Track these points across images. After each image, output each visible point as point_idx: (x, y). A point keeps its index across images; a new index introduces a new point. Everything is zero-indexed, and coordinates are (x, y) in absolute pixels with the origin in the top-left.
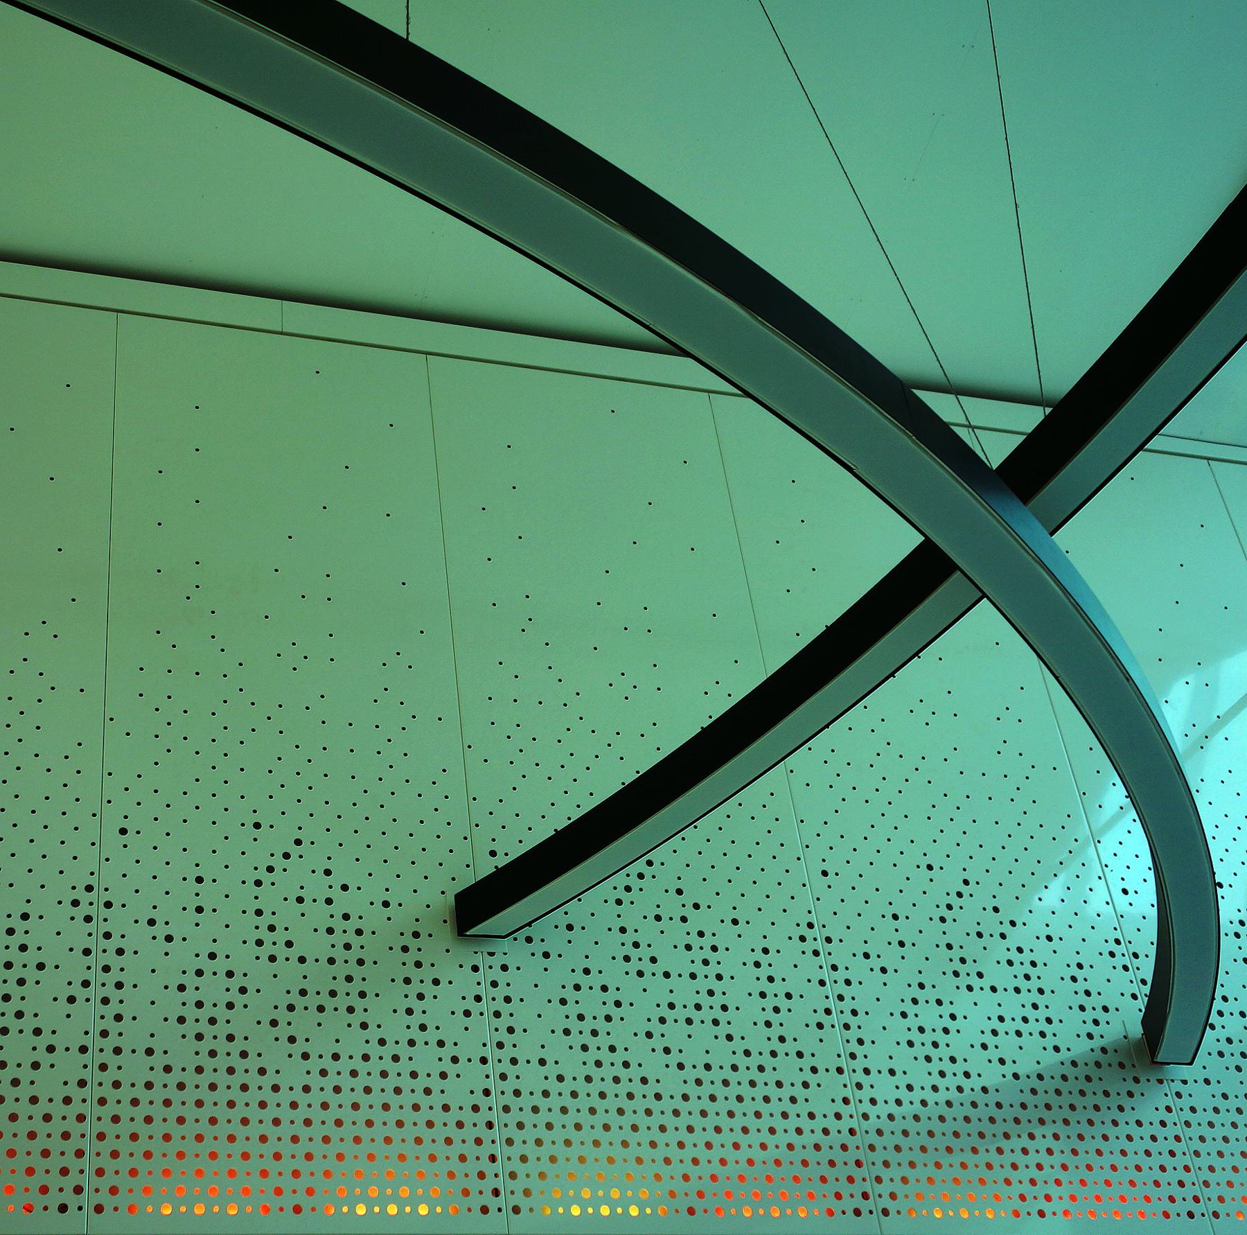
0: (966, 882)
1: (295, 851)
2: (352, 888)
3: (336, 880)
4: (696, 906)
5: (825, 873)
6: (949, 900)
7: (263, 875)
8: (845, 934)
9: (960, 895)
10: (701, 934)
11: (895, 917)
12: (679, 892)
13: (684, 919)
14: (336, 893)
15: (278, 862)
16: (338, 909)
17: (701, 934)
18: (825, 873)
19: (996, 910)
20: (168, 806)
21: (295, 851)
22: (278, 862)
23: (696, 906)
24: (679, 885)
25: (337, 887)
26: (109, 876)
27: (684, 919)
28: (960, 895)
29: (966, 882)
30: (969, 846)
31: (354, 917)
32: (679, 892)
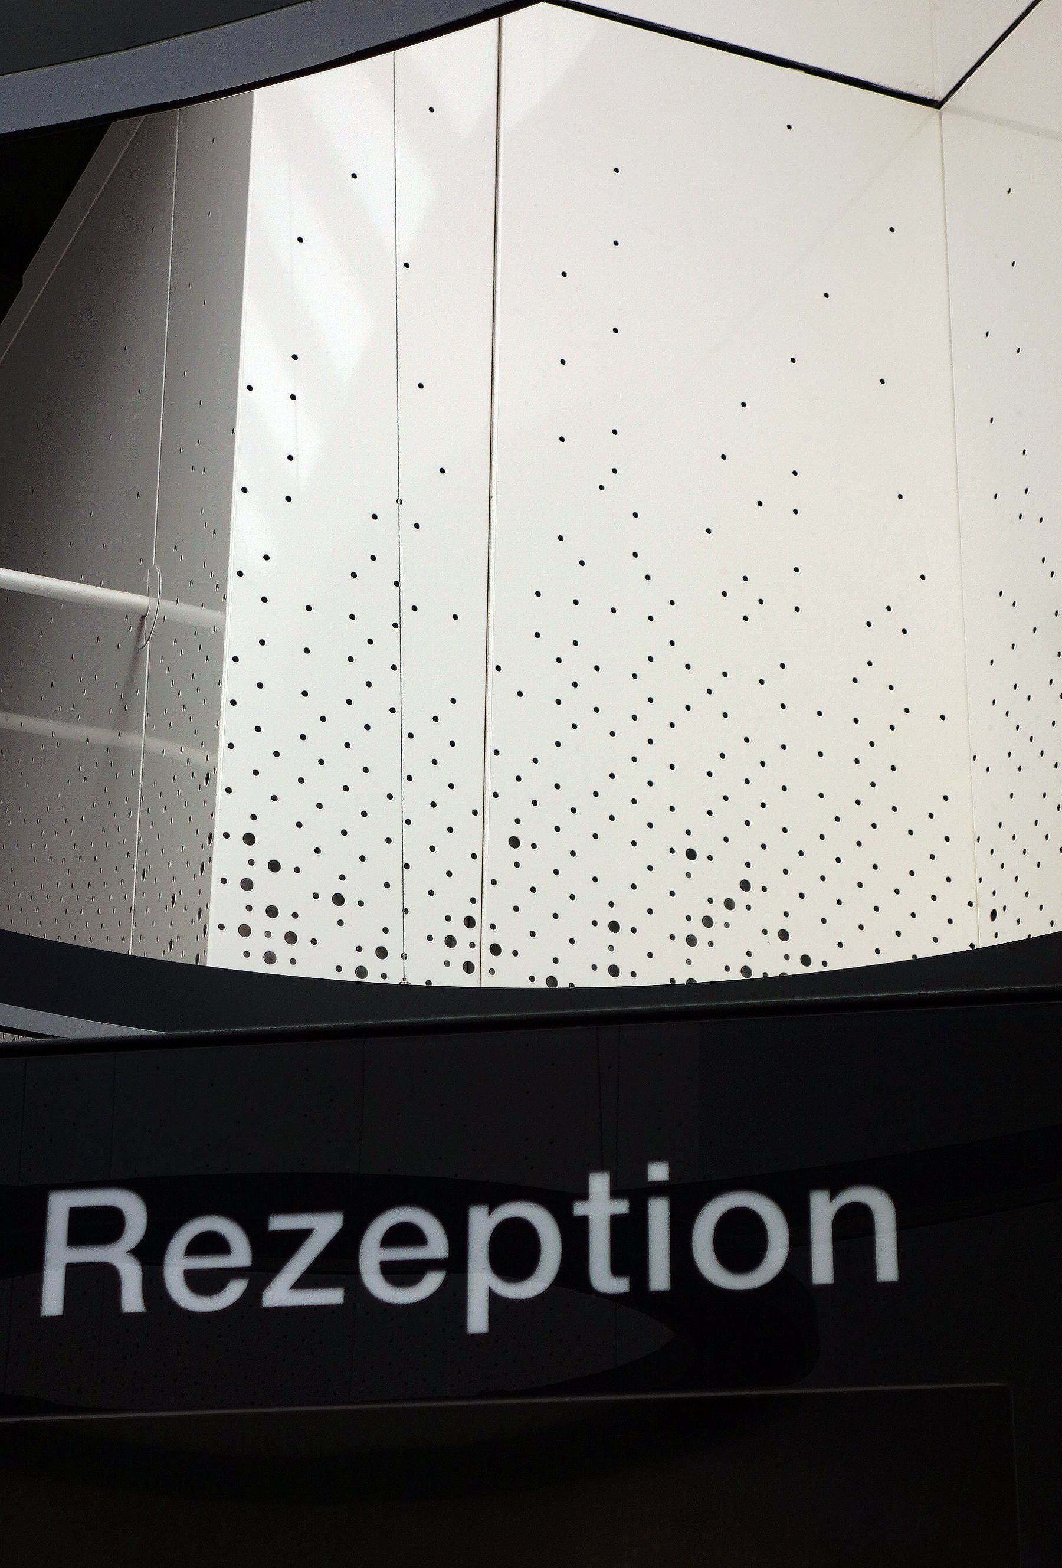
0: (745, 885)
1: (740, 898)
2: (286, 867)
3: (262, 853)
4: (274, 866)
5: (514, 842)
6: (710, 911)
7: (696, 928)
8: (523, 943)
9: (729, 904)
10: (272, 912)
11: (614, 927)
12: (249, 839)
13: (247, 885)
14: (260, 874)
15: (718, 912)
16: (260, 898)
17: (272, 912)
18: (514, 842)
19: (784, 935)
20: (764, 847)
21: (740, 898)
22: (718, 912)
23: (274, 866)
24: (252, 828)
25: (262, 864)
26: (495, 908)
27: (247, 885)
28: (729, 904)
29: (745, 885)
30: (765, 827)
31: (284, 913)
32: (249, 839)
